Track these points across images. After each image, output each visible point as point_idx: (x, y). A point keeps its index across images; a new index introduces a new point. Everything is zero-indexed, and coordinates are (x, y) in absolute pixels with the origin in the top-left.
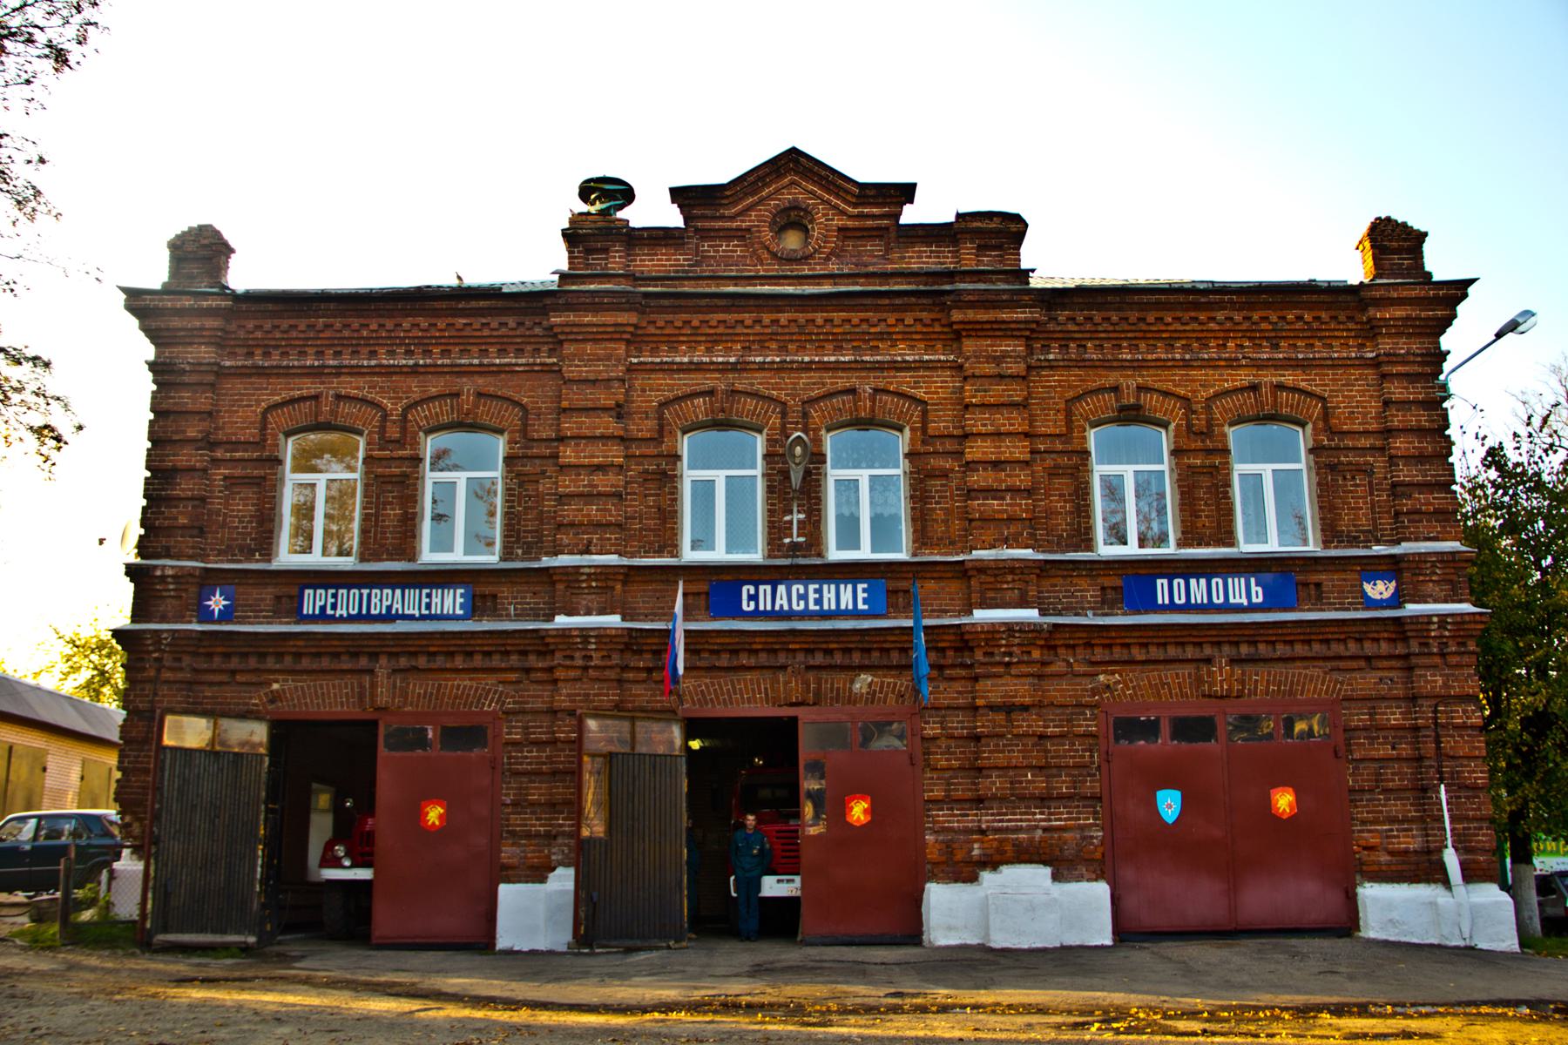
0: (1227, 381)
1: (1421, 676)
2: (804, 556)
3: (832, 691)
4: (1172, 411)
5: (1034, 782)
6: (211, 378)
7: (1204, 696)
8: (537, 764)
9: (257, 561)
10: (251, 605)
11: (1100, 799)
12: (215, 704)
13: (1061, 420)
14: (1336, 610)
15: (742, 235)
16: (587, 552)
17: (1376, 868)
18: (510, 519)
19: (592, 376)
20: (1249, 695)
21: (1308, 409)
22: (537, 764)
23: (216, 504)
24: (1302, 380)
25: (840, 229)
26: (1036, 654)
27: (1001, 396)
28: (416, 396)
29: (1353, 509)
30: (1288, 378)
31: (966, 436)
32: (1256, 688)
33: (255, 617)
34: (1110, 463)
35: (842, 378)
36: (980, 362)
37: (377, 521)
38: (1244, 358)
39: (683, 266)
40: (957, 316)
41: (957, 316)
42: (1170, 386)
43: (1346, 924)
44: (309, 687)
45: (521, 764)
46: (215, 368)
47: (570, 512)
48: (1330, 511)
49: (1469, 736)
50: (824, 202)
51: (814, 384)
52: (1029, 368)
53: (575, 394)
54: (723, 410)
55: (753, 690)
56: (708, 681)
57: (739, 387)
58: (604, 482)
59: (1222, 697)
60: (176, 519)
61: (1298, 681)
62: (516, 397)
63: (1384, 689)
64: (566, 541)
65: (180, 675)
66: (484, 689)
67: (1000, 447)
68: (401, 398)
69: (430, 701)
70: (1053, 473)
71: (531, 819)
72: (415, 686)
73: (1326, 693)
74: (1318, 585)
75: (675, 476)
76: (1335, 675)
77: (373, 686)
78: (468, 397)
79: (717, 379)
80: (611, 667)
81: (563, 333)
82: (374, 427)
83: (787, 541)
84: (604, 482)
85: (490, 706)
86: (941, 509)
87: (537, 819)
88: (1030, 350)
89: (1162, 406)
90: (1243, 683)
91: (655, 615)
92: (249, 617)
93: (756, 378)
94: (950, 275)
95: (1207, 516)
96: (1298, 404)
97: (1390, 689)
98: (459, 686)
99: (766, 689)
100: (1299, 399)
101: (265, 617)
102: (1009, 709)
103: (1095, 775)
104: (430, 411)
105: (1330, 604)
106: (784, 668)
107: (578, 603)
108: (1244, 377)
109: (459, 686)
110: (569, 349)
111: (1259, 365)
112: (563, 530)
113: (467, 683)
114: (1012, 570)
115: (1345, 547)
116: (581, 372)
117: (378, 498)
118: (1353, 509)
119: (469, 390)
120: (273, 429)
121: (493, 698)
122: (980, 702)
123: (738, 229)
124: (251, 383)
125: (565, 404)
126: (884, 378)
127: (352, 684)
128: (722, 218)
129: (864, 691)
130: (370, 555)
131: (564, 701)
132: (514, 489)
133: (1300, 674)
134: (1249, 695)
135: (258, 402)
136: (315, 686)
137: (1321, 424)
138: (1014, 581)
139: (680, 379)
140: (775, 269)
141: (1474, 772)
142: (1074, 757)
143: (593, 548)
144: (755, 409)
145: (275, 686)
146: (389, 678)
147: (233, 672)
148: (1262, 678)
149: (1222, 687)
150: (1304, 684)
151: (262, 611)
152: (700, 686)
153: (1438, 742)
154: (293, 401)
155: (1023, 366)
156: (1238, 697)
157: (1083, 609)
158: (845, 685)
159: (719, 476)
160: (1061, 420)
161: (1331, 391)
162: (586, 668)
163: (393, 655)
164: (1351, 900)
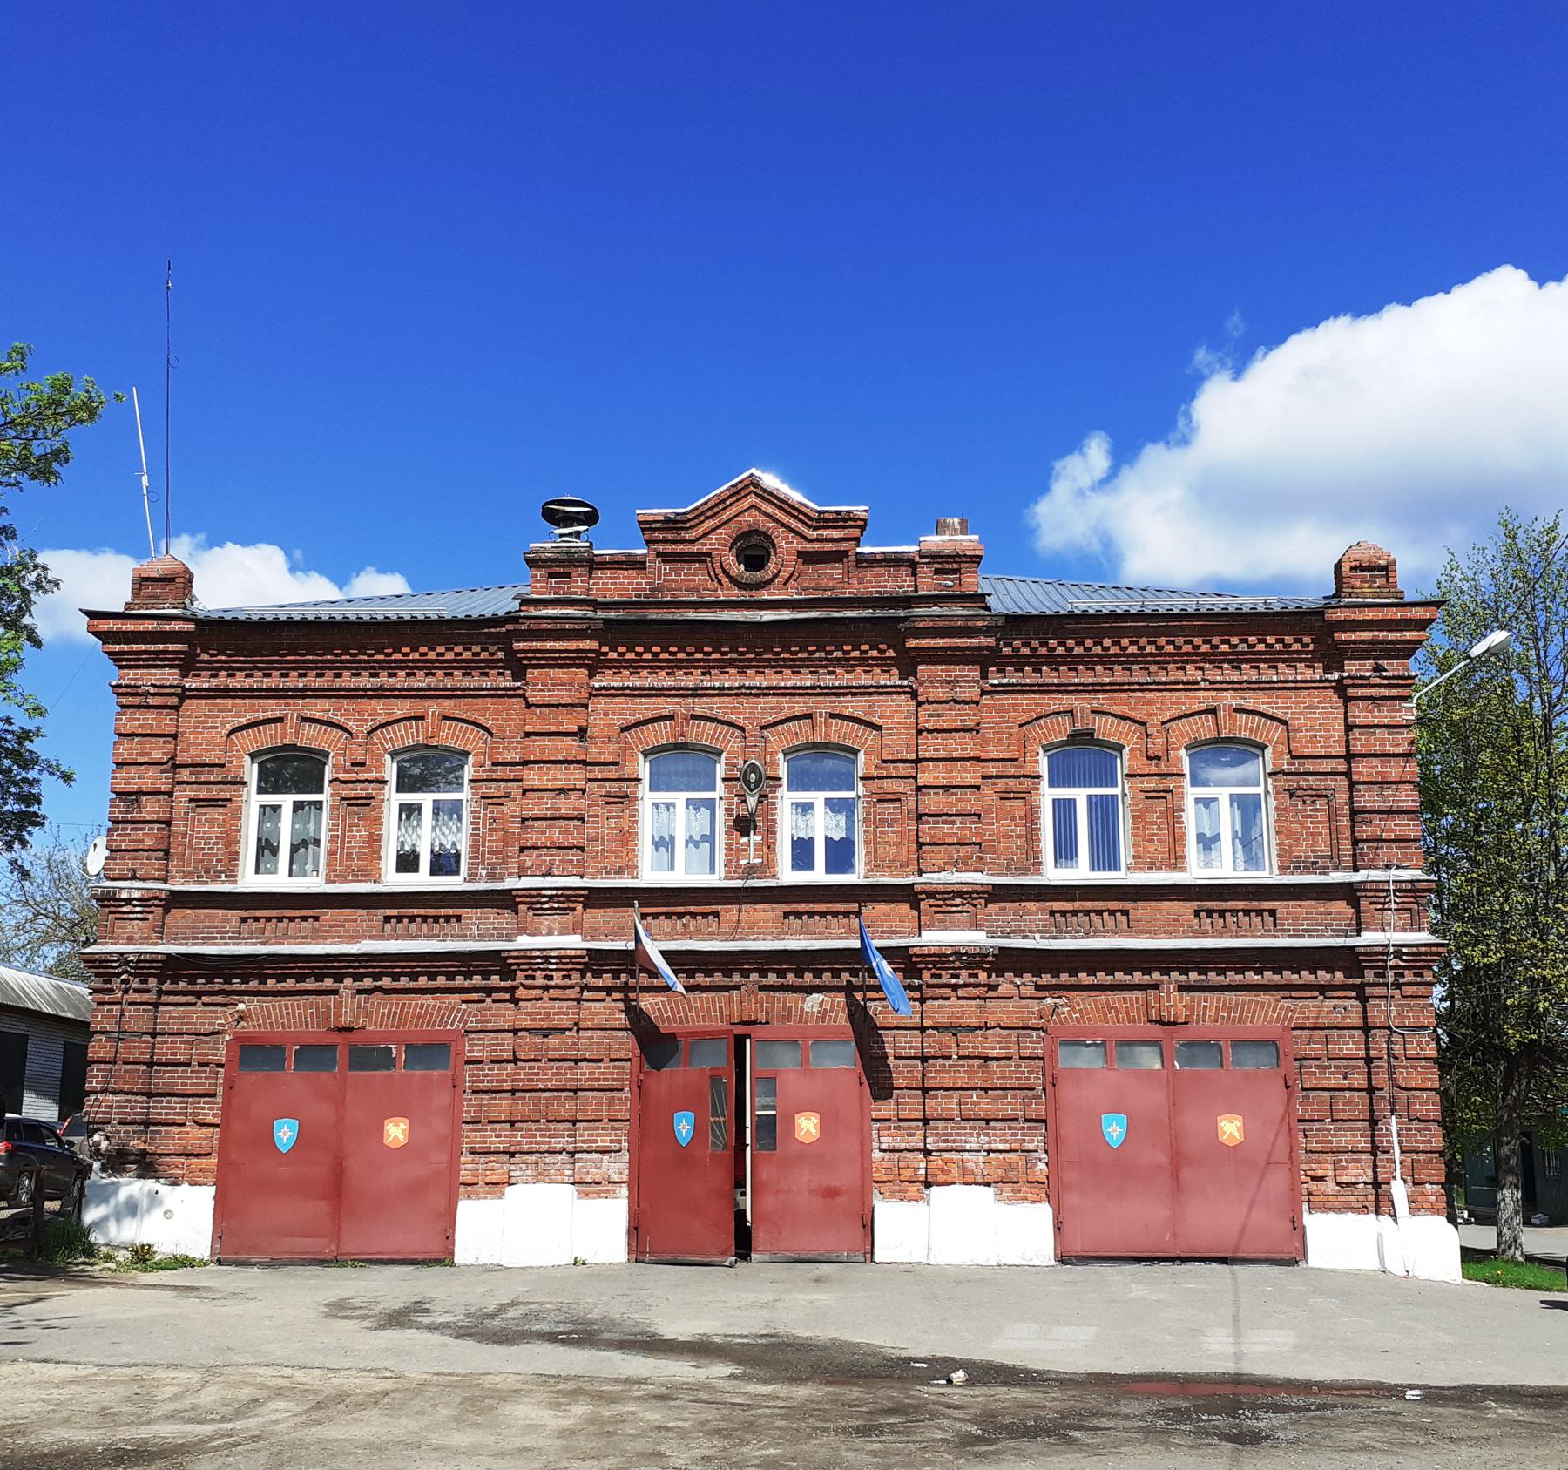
0: (1184, 704)
1: (1374, 1006)
2: (759, 878)
3: (784, 1009)
4: (1127, 735)
5: (979, 1103)
6: (174, 701)
7: (1150, 1021)
8: (497, 1081)
9: (223, 883)
10: (216, 927)
11: (1044, 1121)
12: (182, 1024)
13: (1013, 744)
14: (1290, 937)
15: (701, 557)
16: (549, 874)
17: (1322, 1198)
18: (474, 841)
19: (554, 701)
20: (1198, 1022)
21: (1268, 732)
22: (497, 1081)
23: (179, 826)
24: (1263, 703)
25: (800, 554)
26: (983, 976)
27: (953, 721)
28: (382, 719)
29: (1312, 834)
30: (1249, 700)
31: (918, 761)
32: (1205, 1014)
33: (221, 938)
34: (847, 799)
35: (799, 702)
36: (934, 687)
37: (343, 842)
38: (1204, 680)
39: (645, 589)
40: (911, 643)
41: (911, 643)
42: (1126, 711)
43: (1291, 1255)
44: (274, 1006)
45: (483, 1081)
46: (179, 691)
47: (534, 834)
48: (1288, 837)
49: (1422, 1067)
50: (783, 525)
51: (772, 708)
52: (983, 693)
53: (539, 718)
54: (682, 735)
55: (708, 1008)
56: (665, 999)
57: (698, 712)
58: (565, 805)
59: (1169, 1024)
60: (142, 841)
61: (1249, 1008)
62: (481, 721)
63: (1336, 1019)
64: (529, 863)
65: (146, 997)
66: (447, 1008)
67: (952, 771)
68: (367, 721)
69: (394, 1020)
70: (1005, 796)
71: (490, 1136)
72: (379, 1004)
73: (1277, 1021)
74: (1272, 912)
75: (636, 799)
76: (1286, 1003)
77: (339, 1005)
78: (433, 721)
79: (678, 703)
80: (571, 987)
81: (526, 658)
82: (339, 749)
83: (743, 862)
84: (565, 805)
85: (452, 1024)
86: (893, 832)
87: (497, 1136)
88: (984, 676)
89: (1116, 730)
90: (1192, 1009)
91: (615, 934)
92: (215, 938)
93: (716, 703)
94: (907, 601)
95: (1159, 841)
96: (1258, 727)
97: (1344, 1018)
98: (423, 1005)
99: (720, 1007)
100: (1259, 722)
101: (230, 938)
102: (955, 1030)
103: (1040, 1097)
104: (395, 732)
105: (1284, 930)
106: (737, 987)
107: (541, 924)
108: (1204, 700)
109: (423, 1005)
110: (532, 674)
111: (1217, 687)
112: (526, 852)
113: (433, 1002)
114: (960, 894)
115: (1301, 873)
116: (545, 696)
117: (344, 820)
118: (1312, 834)
119: (434, 713)
120: (238, 751)
121: (455, 1017)
122: (927, 1023)
123: (699, 554)
124: (215, 705)
125: (529, 728)
126: (840, 702)
127: (317, 1003)
128: (683, 541)
129: (815, 1010)
130: (337, 876)
131: (525, 1020)
132: (479, 812)
133: (1251, 1001)
134: (1198, 1022)
135: (223, 724)
136: (280, 1006)
137: (1283, 748)
138: (963, 905)
139: (641, 703)
140: (736, 594)
141: (1426, 1103)
142: (1020, 1079)
143: (555, 871)
144: (715, 733)
145: (241, 1007)
146: (353, 998)
147: (199, 994)
148: (1212, 1004)
149: (1169, 1012)
150: (1254, 1012)
151: (227, 932)
152: (657, 1004)
153: (1391, 1071)
154: (257, 723)
155: (977, 691)
156: (1186, 1023)
157: (1031, 932)
158: (796, 1003)
159: (1080, 795)
160: (1013, 744)
161: (1293, 713)
162: (546, 988)
163: (358, 977)
164: (1298, 1228)
